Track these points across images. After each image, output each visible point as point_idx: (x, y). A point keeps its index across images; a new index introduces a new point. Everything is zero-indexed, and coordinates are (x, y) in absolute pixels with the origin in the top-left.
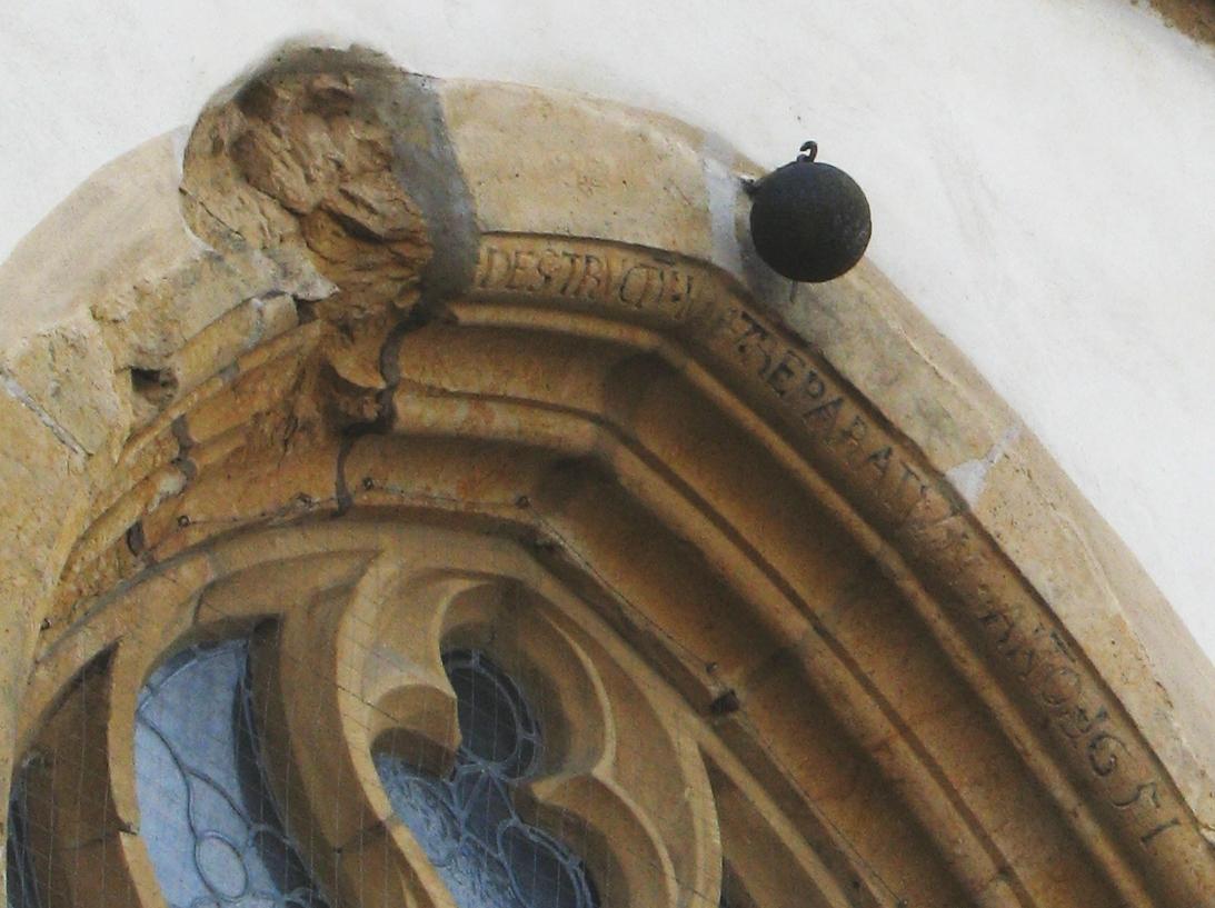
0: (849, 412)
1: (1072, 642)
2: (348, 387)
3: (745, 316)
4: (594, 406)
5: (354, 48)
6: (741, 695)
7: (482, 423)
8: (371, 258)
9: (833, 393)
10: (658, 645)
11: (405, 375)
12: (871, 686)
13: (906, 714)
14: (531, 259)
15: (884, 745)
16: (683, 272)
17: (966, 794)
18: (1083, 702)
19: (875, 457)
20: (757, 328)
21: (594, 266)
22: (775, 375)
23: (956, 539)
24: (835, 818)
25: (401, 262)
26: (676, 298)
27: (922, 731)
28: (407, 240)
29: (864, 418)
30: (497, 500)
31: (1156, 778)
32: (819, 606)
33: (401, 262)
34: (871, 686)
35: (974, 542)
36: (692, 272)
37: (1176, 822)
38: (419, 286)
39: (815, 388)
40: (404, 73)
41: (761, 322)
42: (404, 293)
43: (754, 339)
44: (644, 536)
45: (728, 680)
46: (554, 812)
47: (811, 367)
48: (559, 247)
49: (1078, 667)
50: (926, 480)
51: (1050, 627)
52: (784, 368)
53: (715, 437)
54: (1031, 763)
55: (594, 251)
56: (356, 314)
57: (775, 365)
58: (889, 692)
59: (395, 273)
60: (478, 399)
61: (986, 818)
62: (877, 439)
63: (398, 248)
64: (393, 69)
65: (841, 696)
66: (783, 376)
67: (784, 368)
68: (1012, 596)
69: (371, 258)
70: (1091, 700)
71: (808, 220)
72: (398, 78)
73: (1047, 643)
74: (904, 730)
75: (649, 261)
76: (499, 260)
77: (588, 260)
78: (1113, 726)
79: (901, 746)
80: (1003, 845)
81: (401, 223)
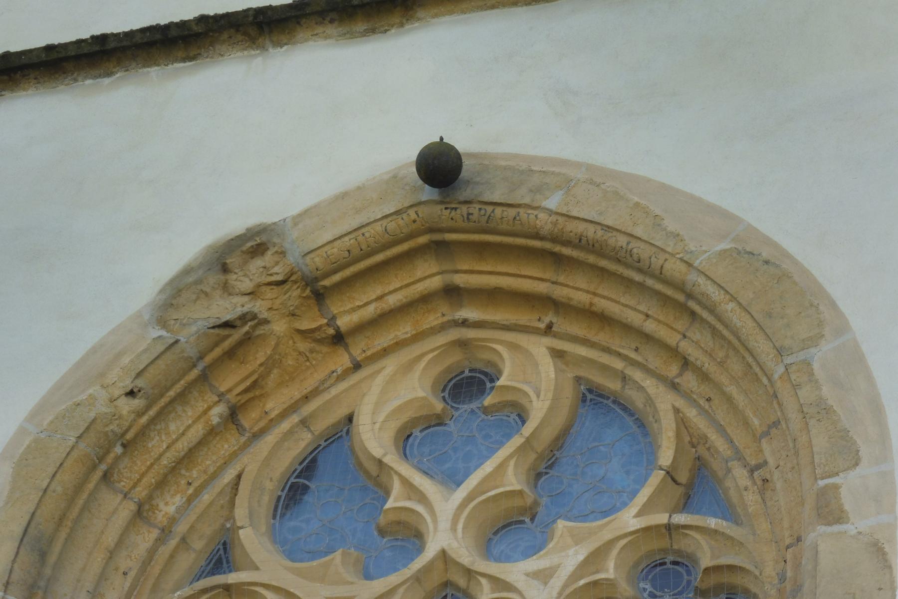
0: (498, 211)
1: (608, 227)
2: (313, 331)
3: (446, 208)
4: (434, 270)
5: (247, 229)
6: (554, 320)
7: (384, 305)
8: (287, 287)
9: (489, 209)
10: (516, 325)
11: (335, 312)
12: (576, 288)
13: (592, 289)
14: (334, 251)
15: (591, 304)
16: (412, 212)
17: (623, 300)
18: (620, 244)
19: (515, 218)
20: (453, 209)
21: (367, 235)
22: (468, 218)
23: (555, 224)
24: (602, 337)
25: (295, 282)
26: (414, 221)
27: (600, 291)
28: (292, 275)
29: (505, 209)
30: (432, 320)
31: (654, 250)
32: (547, 276)
33: (295, 282)
34: (576, 288)
35: (561, 220)
36: (415, 209)
37: (666, 260)
38: (307, 285)
39: (483, 212)
40: (275, 224)
41: (454, 206)
42: (304, 290)
43: (453, 213)
44: (492, 296)
45: (549, 318)
46: (494, 405)
47: (478, 206)
48: (346, 239)
49: (615, 233)
50: (535, 212)
51: (599, 228)
52: (469, 214)
53: (481, 250)
54: (625, 275)
55: (363, 230)
56: (291, 308)
57: (465, 216)
58: (583, 286)
59: (295, 287)
60: (380, 298)
61: (632, 303)
62: (512, 212)
63: (292, 279)
64: (270, 225)
65: (570, 299)
66: (470, 217)
67: (469, 214)
68: (581, 227)
69: (287, 287)
70: (622, 241)
71: (440, 168)
72: (273, 227)
73: (600, 233)
74: (595, 294)
75: (395, 217)
76: (317, 259)
77: (363, 235)
78: (634, 244)
79: (596, 300)
80: (642, 308)
81: (287, 271)
